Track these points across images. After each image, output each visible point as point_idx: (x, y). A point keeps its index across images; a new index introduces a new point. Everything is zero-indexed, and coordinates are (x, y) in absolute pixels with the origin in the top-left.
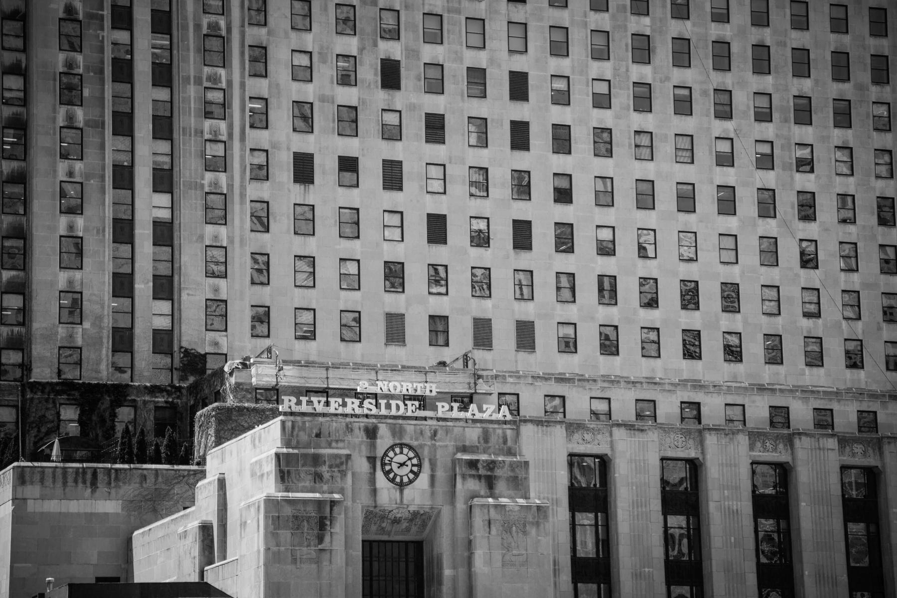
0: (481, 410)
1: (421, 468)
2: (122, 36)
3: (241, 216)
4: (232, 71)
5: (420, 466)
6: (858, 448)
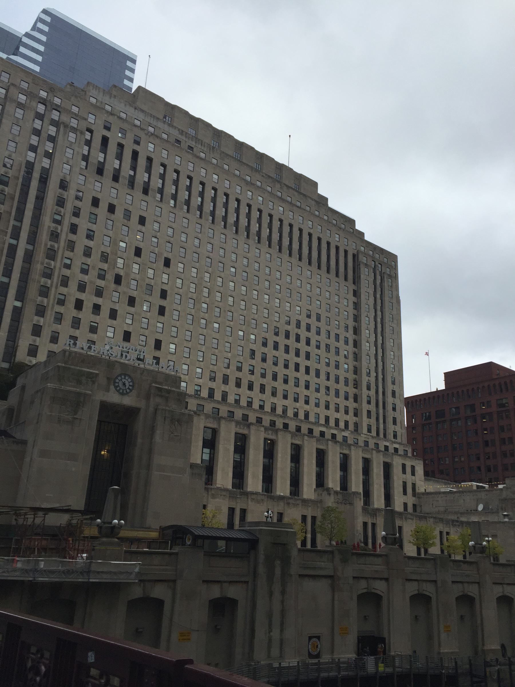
1: (134, 387)
2: (14, 242)
3: (50, 315)
6: (270, 432)
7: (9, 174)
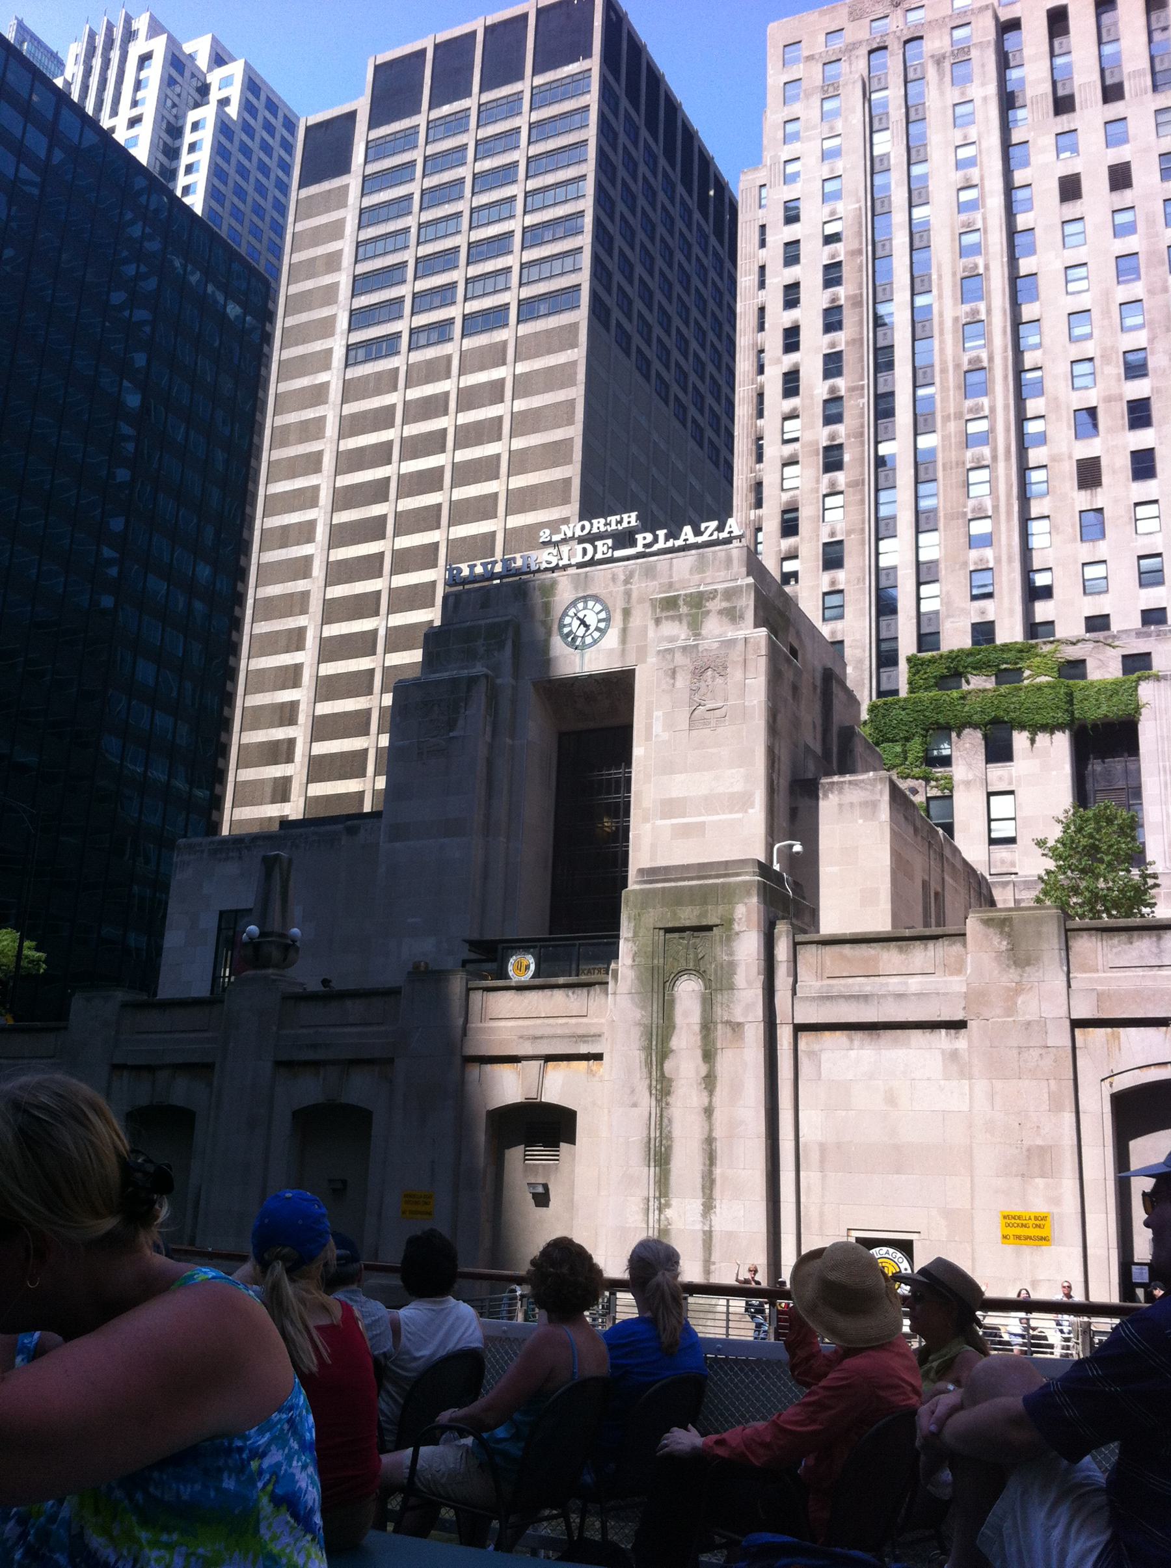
0: (698, 532)
4: (994, 397)
5: (607, 620)
7: (839, 256)
